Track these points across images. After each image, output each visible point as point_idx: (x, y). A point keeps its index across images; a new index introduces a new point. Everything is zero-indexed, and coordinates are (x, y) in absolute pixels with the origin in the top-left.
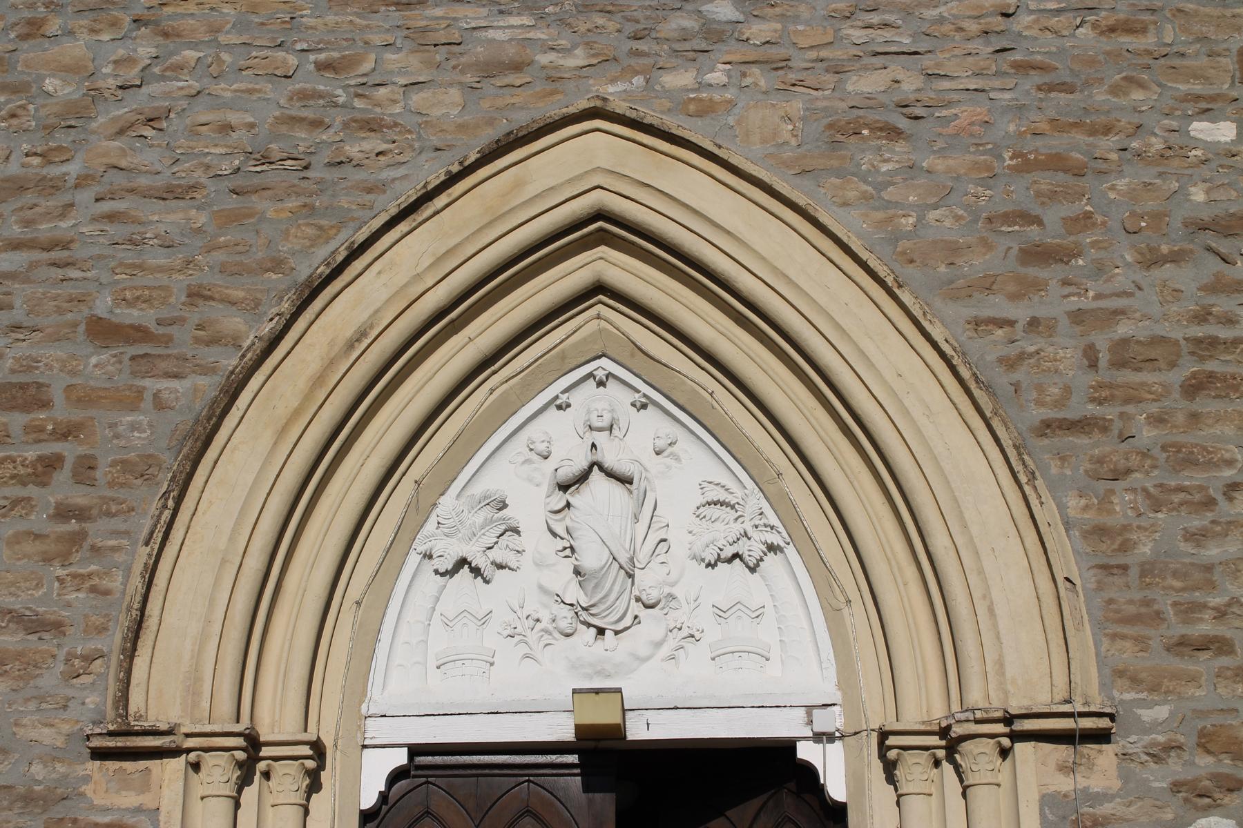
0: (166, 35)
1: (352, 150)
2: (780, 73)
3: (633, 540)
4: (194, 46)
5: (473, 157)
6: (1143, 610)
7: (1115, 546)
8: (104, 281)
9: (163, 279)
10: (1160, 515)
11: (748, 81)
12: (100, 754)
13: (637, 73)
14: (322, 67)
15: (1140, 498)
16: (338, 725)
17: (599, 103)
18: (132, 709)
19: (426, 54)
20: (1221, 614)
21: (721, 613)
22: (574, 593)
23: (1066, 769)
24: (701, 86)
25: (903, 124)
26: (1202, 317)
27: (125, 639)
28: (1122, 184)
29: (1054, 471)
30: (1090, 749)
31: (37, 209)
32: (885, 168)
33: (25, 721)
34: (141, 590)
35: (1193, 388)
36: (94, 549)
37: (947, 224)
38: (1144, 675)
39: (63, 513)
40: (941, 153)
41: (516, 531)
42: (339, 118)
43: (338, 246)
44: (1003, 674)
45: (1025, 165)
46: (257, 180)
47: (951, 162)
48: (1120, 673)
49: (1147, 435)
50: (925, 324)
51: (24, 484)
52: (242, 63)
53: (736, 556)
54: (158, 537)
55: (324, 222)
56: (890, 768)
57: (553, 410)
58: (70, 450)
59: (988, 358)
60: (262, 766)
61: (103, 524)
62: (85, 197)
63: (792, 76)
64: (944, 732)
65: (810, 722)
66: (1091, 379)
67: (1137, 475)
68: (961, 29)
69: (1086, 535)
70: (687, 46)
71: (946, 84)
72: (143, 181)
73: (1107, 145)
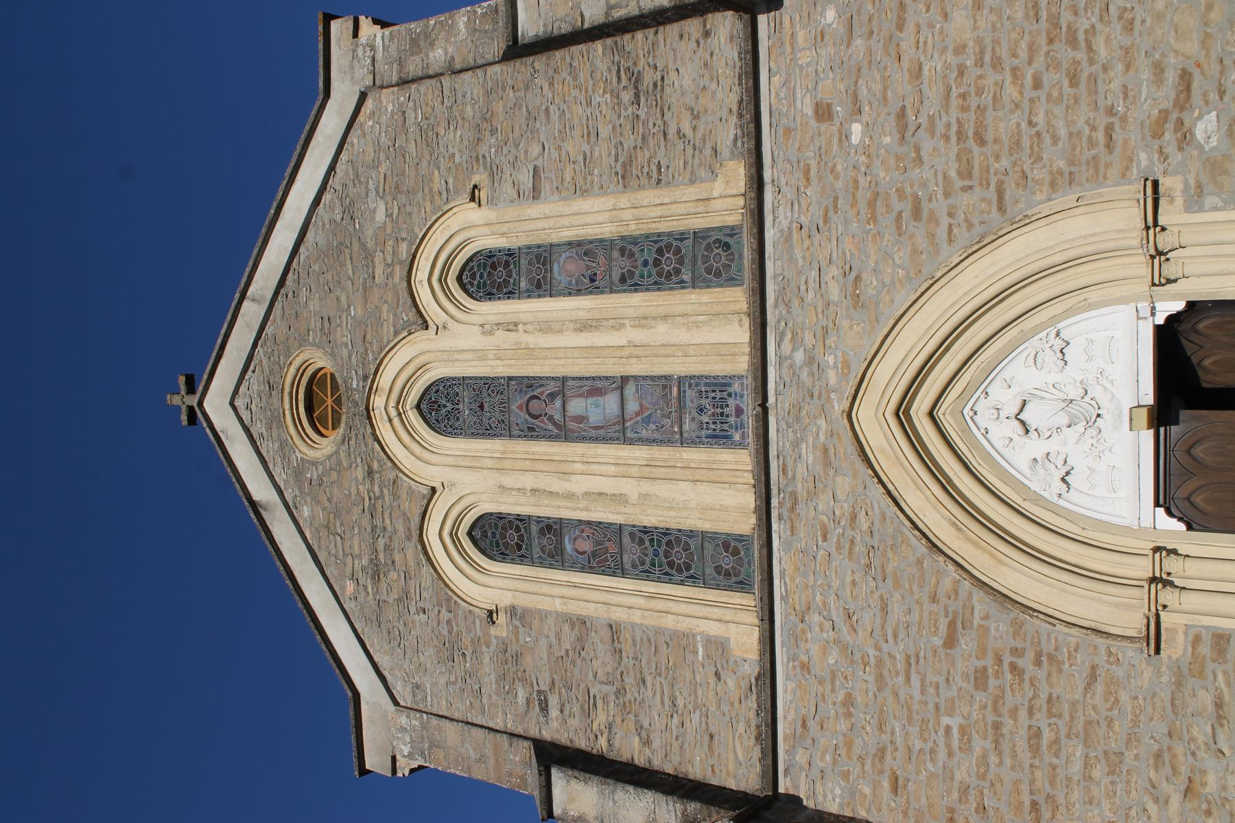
0: (809, 608)
1: (865, 526)
2: (829, 330)
3: (1052, 400)
4: (814, 597)
5: (870, 472)
6: (1092, 165)
7: (1060, 177)
8: (926, 640)
9: (925, 614)
10: (1045, 157)
11: (833, 345)
12: (1158, 650)
13: (829, 397)
14: (825, 539)
15: (1036, 166)
16: (1143, 540)
17: (845, 414)
18: (1136, 635)
19: (820, 492)
20: (1094, 129)
21: (1090, 359)
22: (1080, 428)
23: (1172, 201)
24: (835, 366)
25: (853, 275)
26: (946, 138)
27: (1101, 637)
28: (882, 175)
29: (1023, 206)
30: (1161, 189)
31: (891, 669)
32: (875, 283)
33: (1140, 684)
34: (1078, 629)
35: (981, 141)
36: (1056, 649)
37: (902, 254)
38: (1125, 164)
39: (1038, 663)
40: (867, 257)
41: (1048, 454)
42: (850, 532)
43: (912, 535)
44: (1125, 230)
45: (873, 218)
46: (879, 570)
47: (872, 252)
48: (1123, 176)
49: (1005, 163)
50: (952, 265)
51: (1024, 680)
52: (823, 575)
53: (1061, 351)
54: (1051, 620)
55: (900, 540)
56: (1169, 281)
57: (988, 436)
58: (1007, 659)
59: (967, 236)
60: (1164, 576)
61: (1044, 646)
62: (885, 648)
63: (831, 325)
64: (1153, 257)
65: (1146, 318)
66: (977, 189)
67: (1024, 167)
68: (808, 249)
69: (1054, 191)
70: (816, 373)
71: (835, 255)
72: (878, 622)
73: (863, 181)
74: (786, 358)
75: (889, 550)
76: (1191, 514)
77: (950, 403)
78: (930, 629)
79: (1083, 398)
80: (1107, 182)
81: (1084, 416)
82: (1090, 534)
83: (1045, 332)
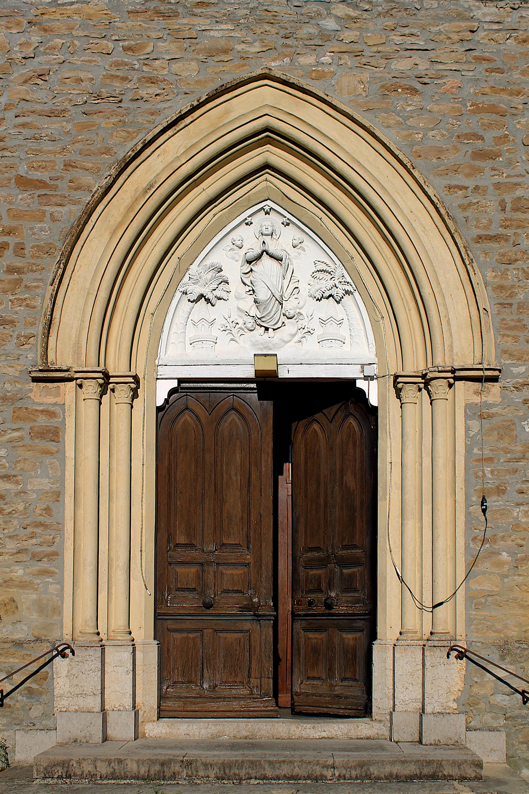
1: (143, 93)
2: (358, 58)
4: (60, 36)
6: (517, 324)
9: (52, 157)
11: (342, 62)
12: (35, 380)
13: (286, 56)
17: (267, 71)
18: (50, 360)
21: (323, 322)
22: (254, 311)
23: (478, 393)
24: (318, 64)
25: (419, 86)
29: (482, 259)
30: (489, 385)
37: (438, 138)
39: (11, 270)
41: (228, 283)
42: (135, 76)
43: (137, 142)
45: (477, 109)
46: (95, 108)
48: (505, 352)
52: (86, 47)
53: (331, 296)
54: (57, 281)
55: (130, 130)
58: (11, 240)
60: (111, 386)
63: (364, 60)
64: (424, 376)
65: (363, 371)
66: (502, 216)
67: (520, 262)
70: (312, 42)
71: (441, 67)
72: (38, 107)
74: (328, 9)
75: (119, 118)
76: (173, 412)
77: (279, 186)
78: (36, 162)
79: (284, 315)
80: (500, 338)
81: (266, 315)
82: (174, 261)
83: (350, 281)
